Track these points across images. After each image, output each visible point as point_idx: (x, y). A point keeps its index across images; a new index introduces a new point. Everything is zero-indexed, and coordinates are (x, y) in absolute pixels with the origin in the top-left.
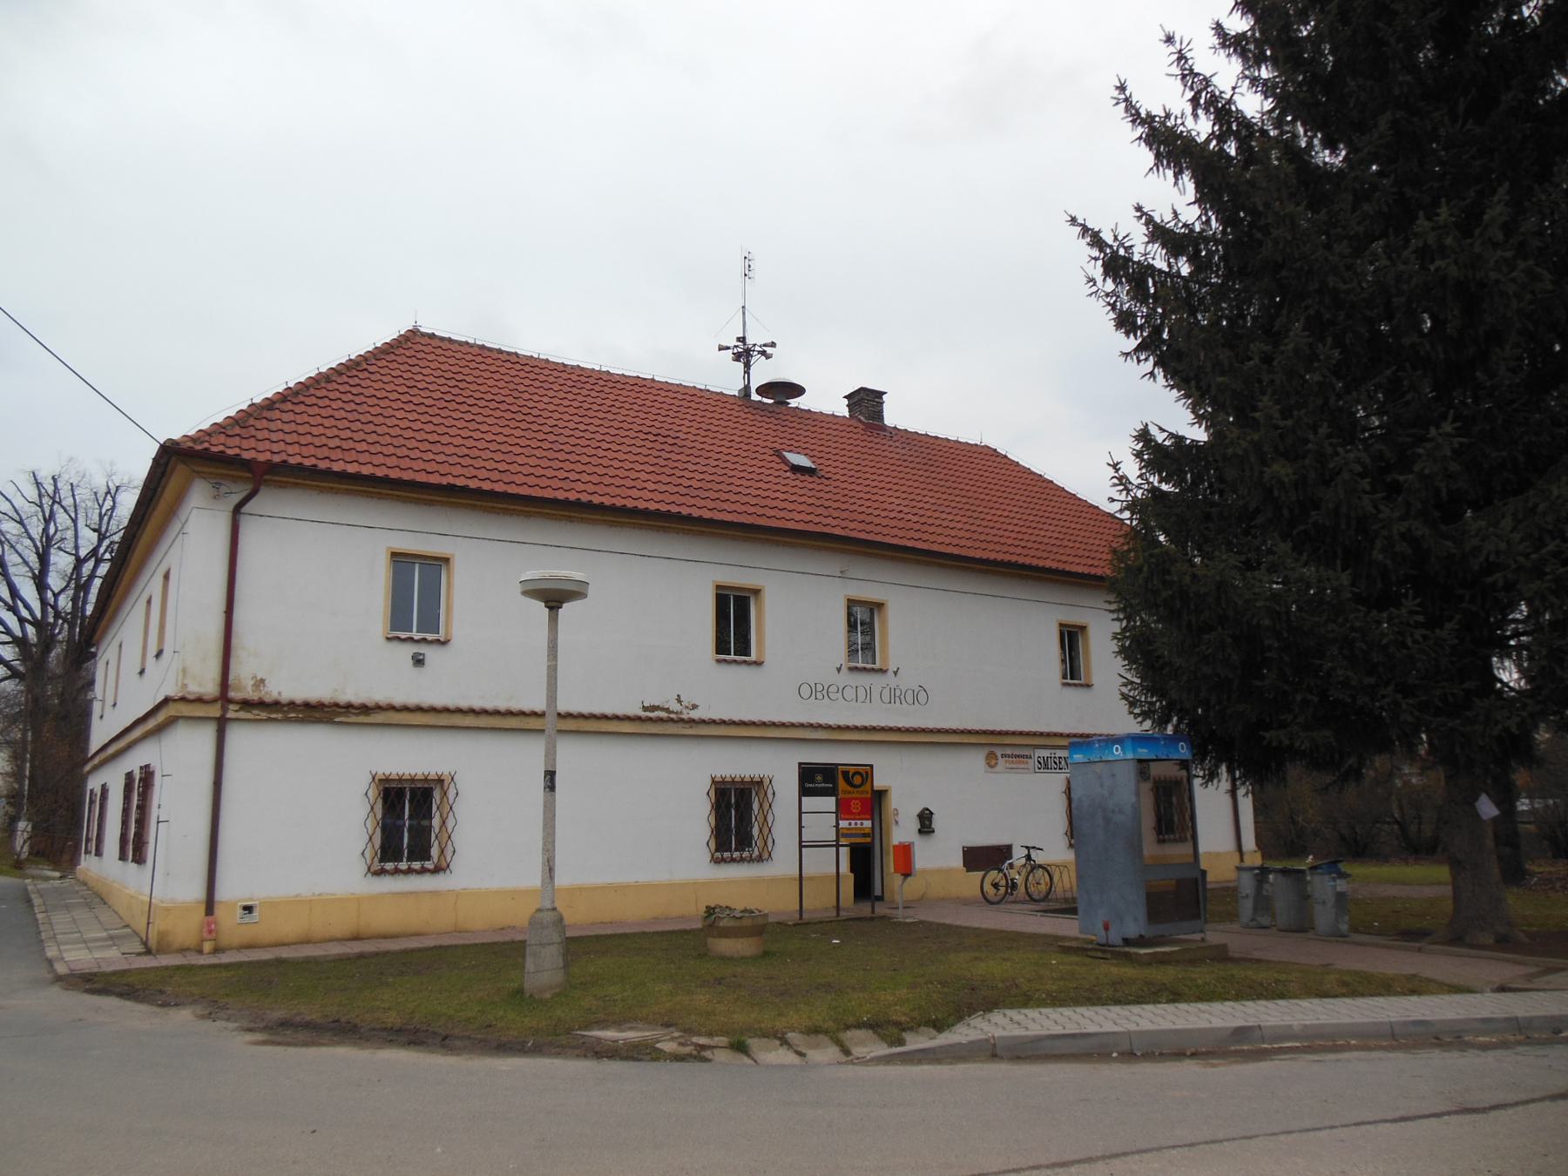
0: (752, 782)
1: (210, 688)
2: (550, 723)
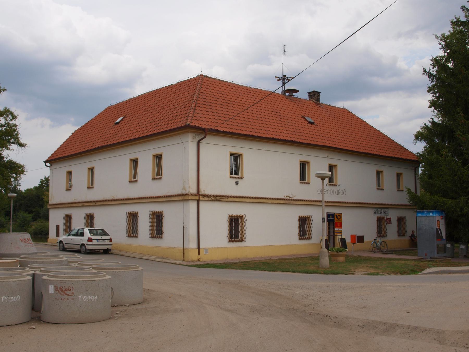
0: (240, 216)
1: (194, 191)
2: (324, 204)
